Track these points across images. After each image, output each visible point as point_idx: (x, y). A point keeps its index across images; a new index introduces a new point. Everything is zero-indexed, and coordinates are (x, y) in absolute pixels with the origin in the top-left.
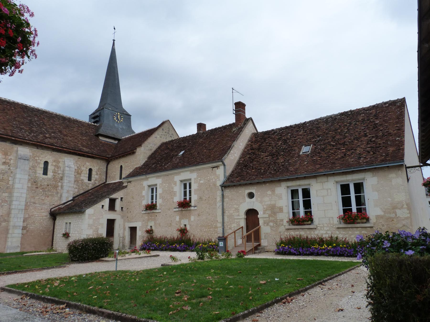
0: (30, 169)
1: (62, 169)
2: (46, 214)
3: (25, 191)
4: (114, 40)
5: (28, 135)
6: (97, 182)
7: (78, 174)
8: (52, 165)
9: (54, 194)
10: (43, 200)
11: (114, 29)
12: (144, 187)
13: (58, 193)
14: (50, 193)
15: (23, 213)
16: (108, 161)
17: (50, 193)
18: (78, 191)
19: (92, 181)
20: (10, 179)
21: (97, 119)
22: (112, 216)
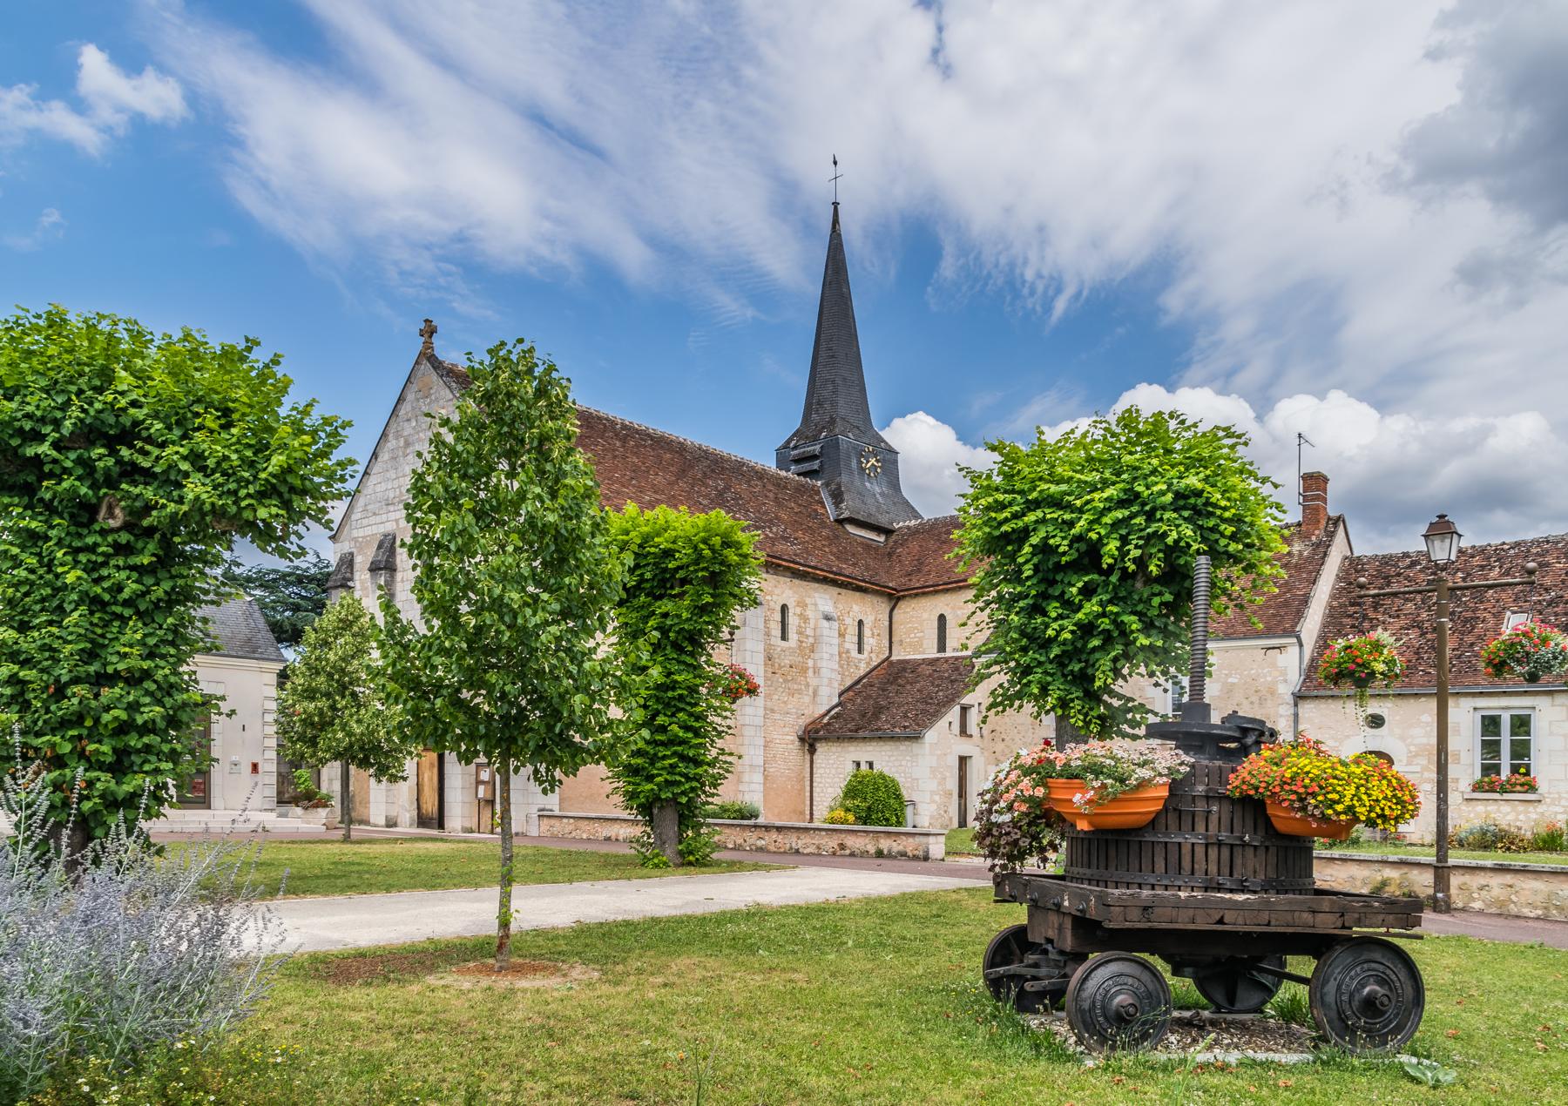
4: (836, 204)
13: (808, 685)
16: (894, 598)
21: (816, 465)
22: (965, 747)
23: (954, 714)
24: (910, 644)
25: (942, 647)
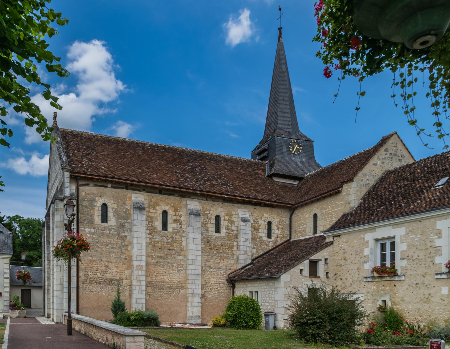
0: (202, 226)
1: (236, 225)
2: (223, 280)
3: (200, 253)
4: (280, 29)
5: (194, 185)
6: (279, 239)
7: (255, 229)
8: (224, 220)
9: (230, 256)
10: (218, 263)
11: (280, 9)
12: (367, 242)
13: (233, 255)
14: (225, 255)
15: (200, 279)
16: (292, 209)
17: (225, 255)
18: (257, 252)
19: (273, 238)
20: (183, 239)
21: (265, 154)
23: (305, 265)
24: (300, 232)
25: (315, 231)
